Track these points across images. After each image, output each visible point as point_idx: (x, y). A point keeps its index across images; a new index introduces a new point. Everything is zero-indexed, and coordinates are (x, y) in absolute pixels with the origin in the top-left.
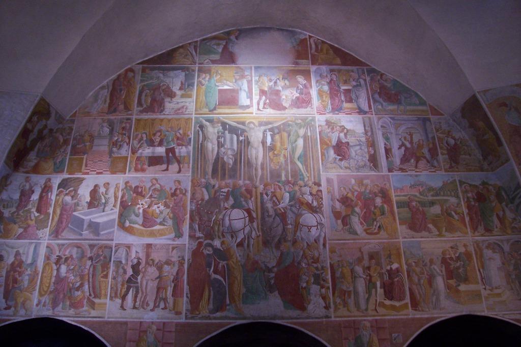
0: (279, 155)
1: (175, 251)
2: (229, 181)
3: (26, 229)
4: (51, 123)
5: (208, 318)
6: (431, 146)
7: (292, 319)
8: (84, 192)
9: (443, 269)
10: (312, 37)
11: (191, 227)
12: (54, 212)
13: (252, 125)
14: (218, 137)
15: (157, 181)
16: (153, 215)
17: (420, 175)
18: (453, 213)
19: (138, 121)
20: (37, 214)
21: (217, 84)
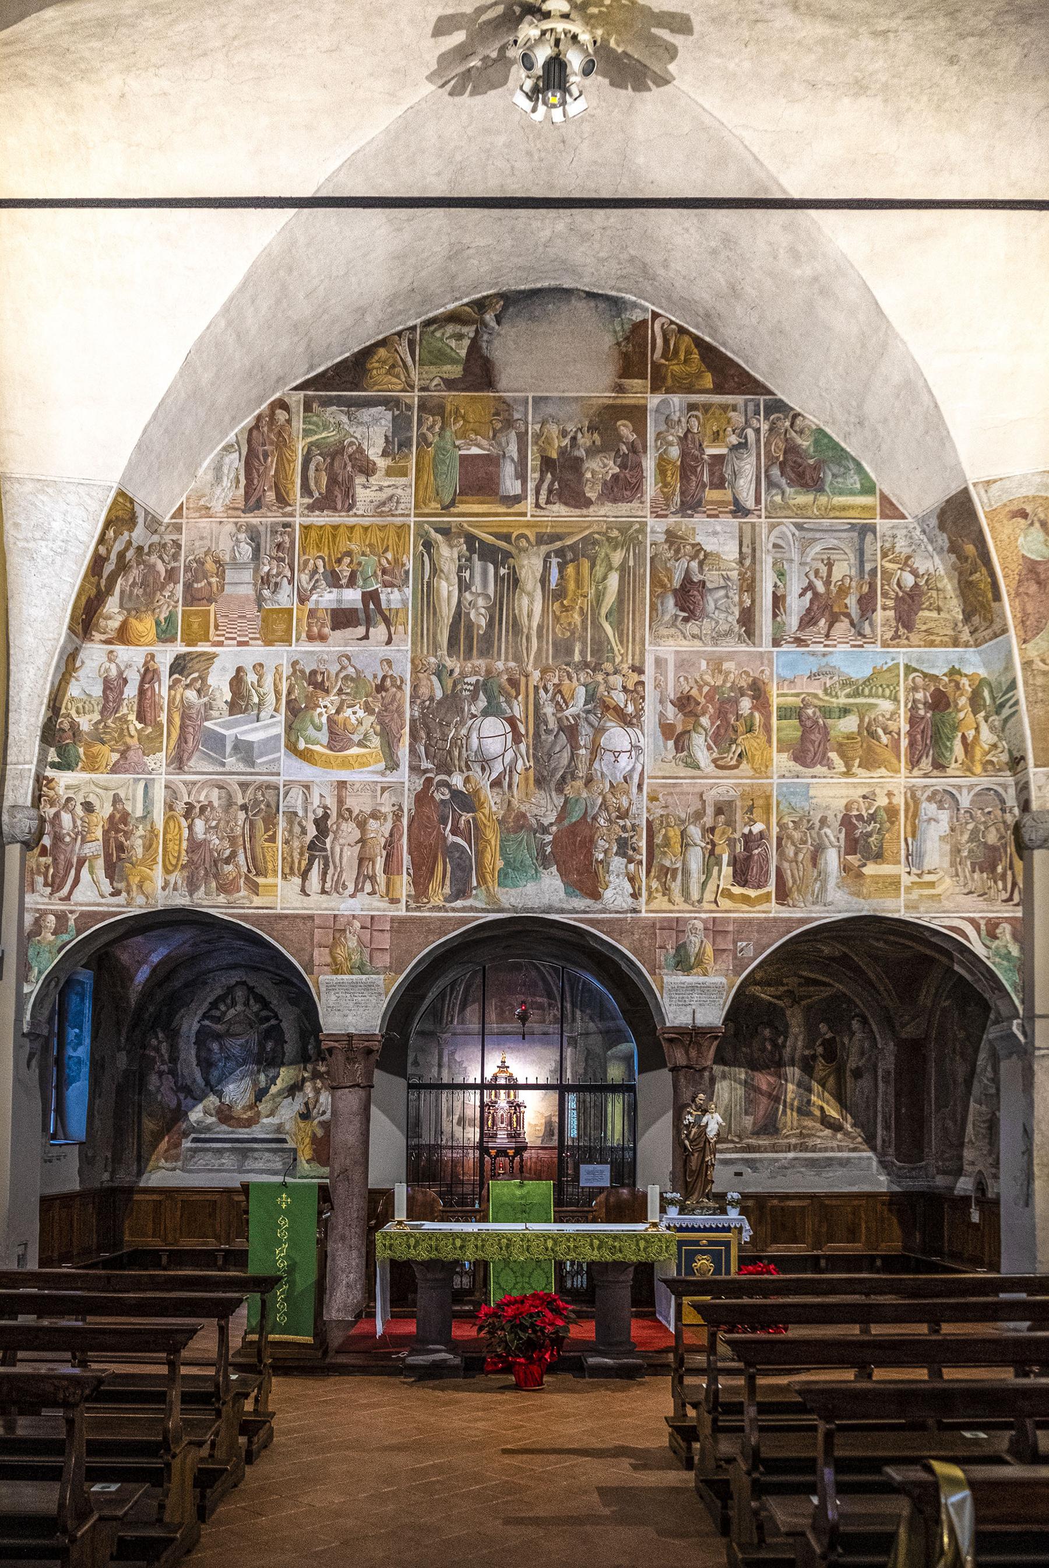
0: (573, 608)
1: (386, 794)
2: (481, 663)
3: (124, 754)
4: (139, 534)
5: (439, 909)
6: (865, 589)
7: (577, 912)
8: (219, 681)
9: (842, 836)
10: (659, 315)
11: (413, 751)
12: (170, 721)
13: (523, 543)
14: (460, 569)
15: (349, 659)
16: (345, 728)
17: (831, 653)
18: (880, 731)
19: (306, 528)
20: (139, 726)
21: (457, 443)
